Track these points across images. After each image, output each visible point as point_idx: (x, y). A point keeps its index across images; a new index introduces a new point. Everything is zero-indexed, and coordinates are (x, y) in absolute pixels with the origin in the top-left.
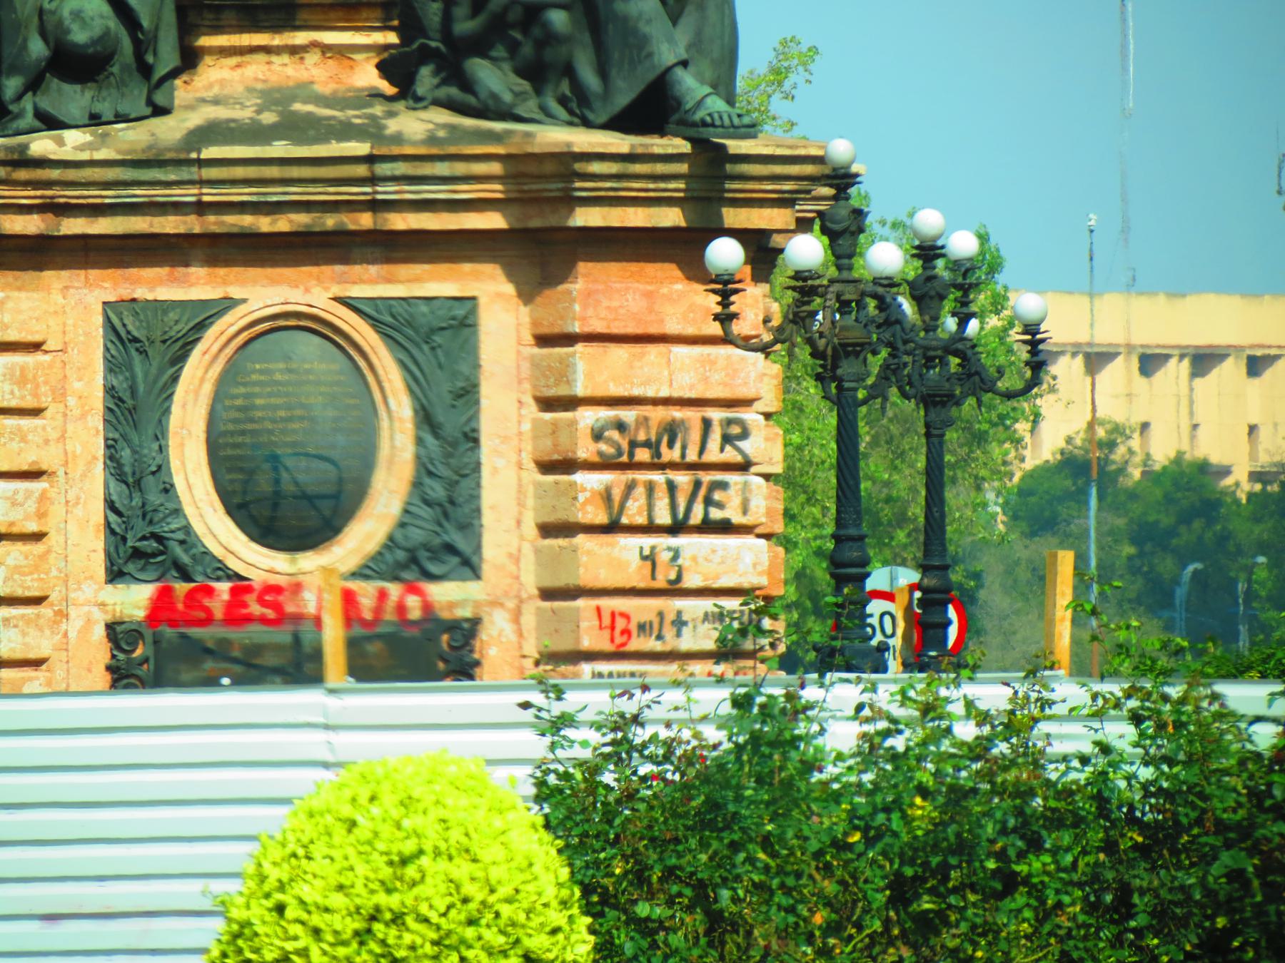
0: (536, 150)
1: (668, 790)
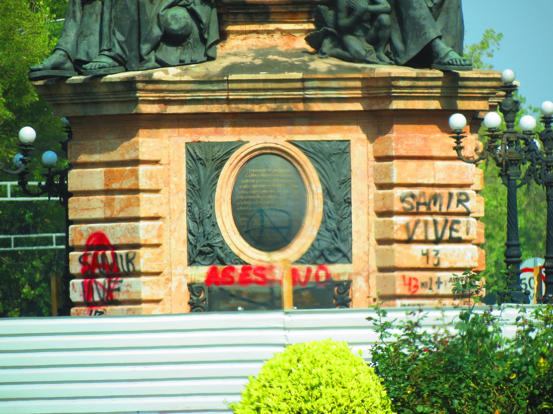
0: (375, 76)
1: (431, 356)
